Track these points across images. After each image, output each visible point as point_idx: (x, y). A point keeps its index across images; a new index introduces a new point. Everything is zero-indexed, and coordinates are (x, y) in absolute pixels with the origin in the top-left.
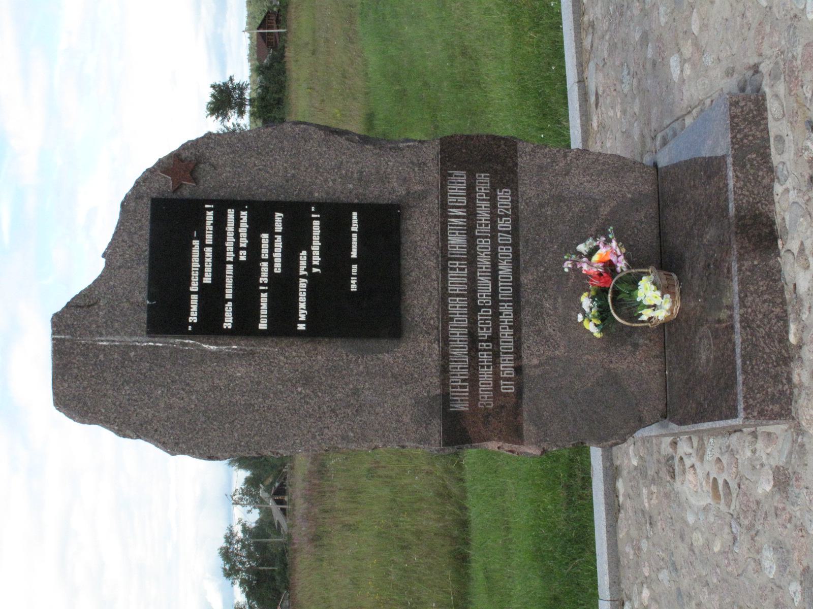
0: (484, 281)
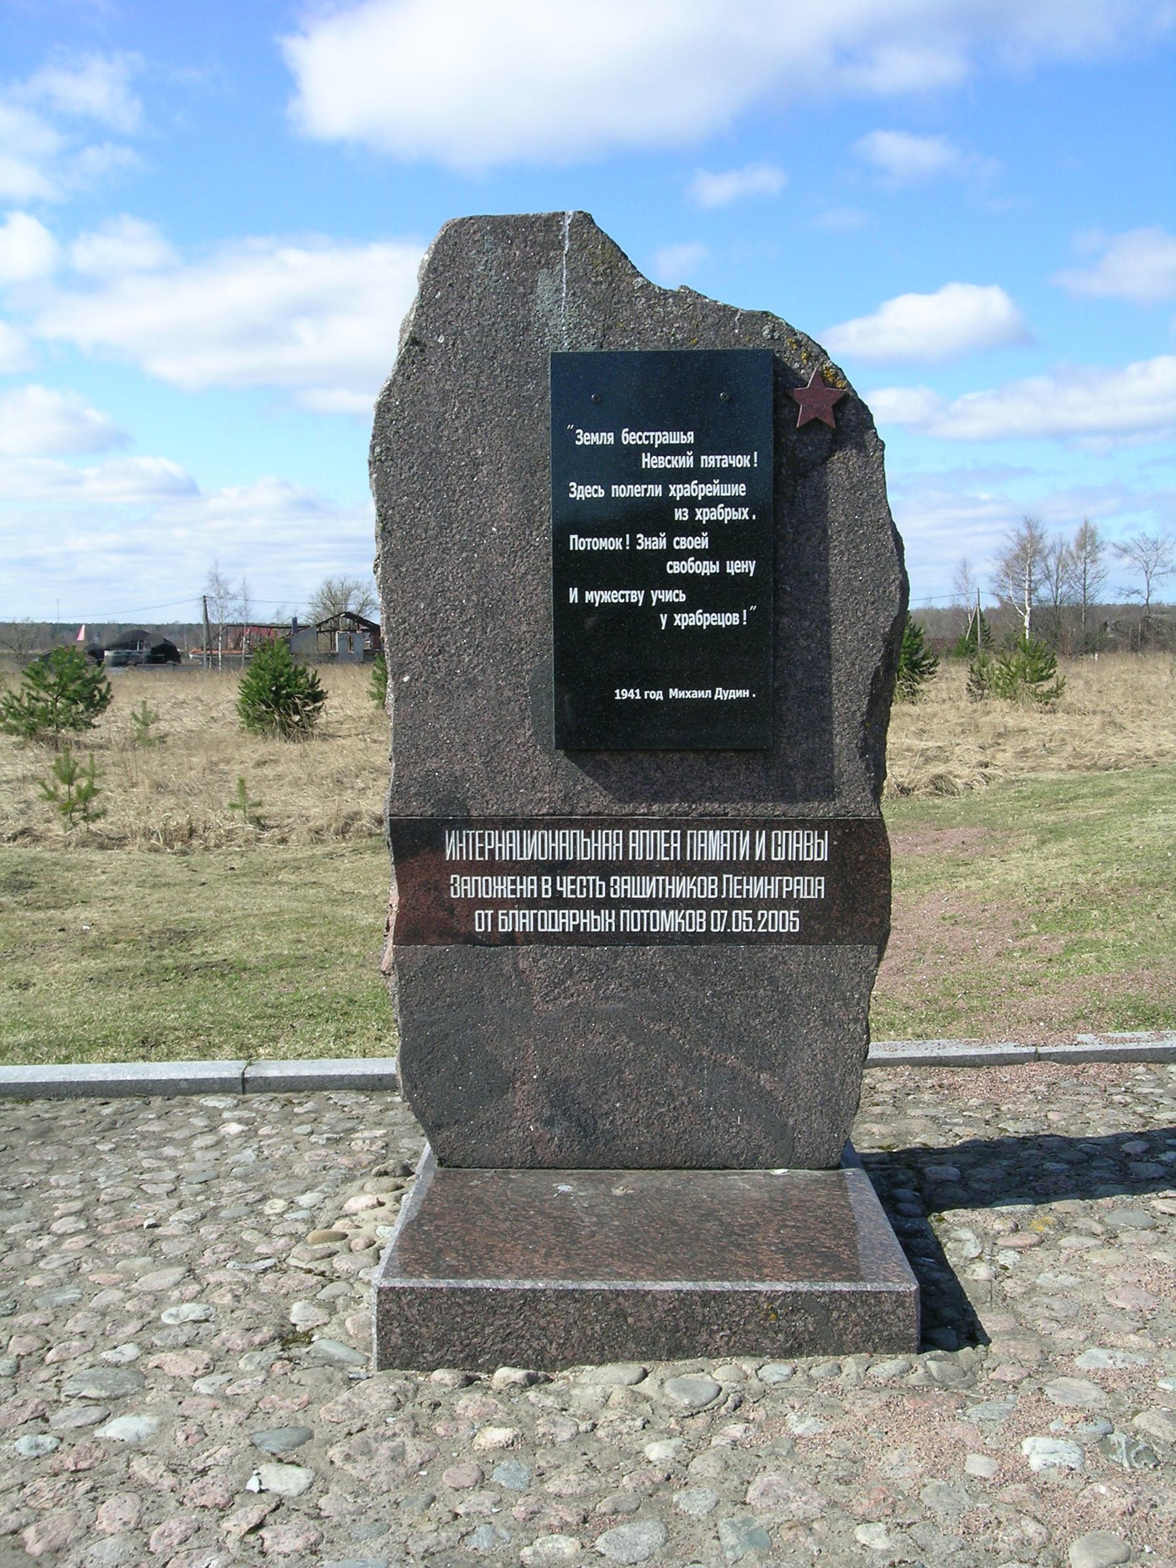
0: (648, 887)
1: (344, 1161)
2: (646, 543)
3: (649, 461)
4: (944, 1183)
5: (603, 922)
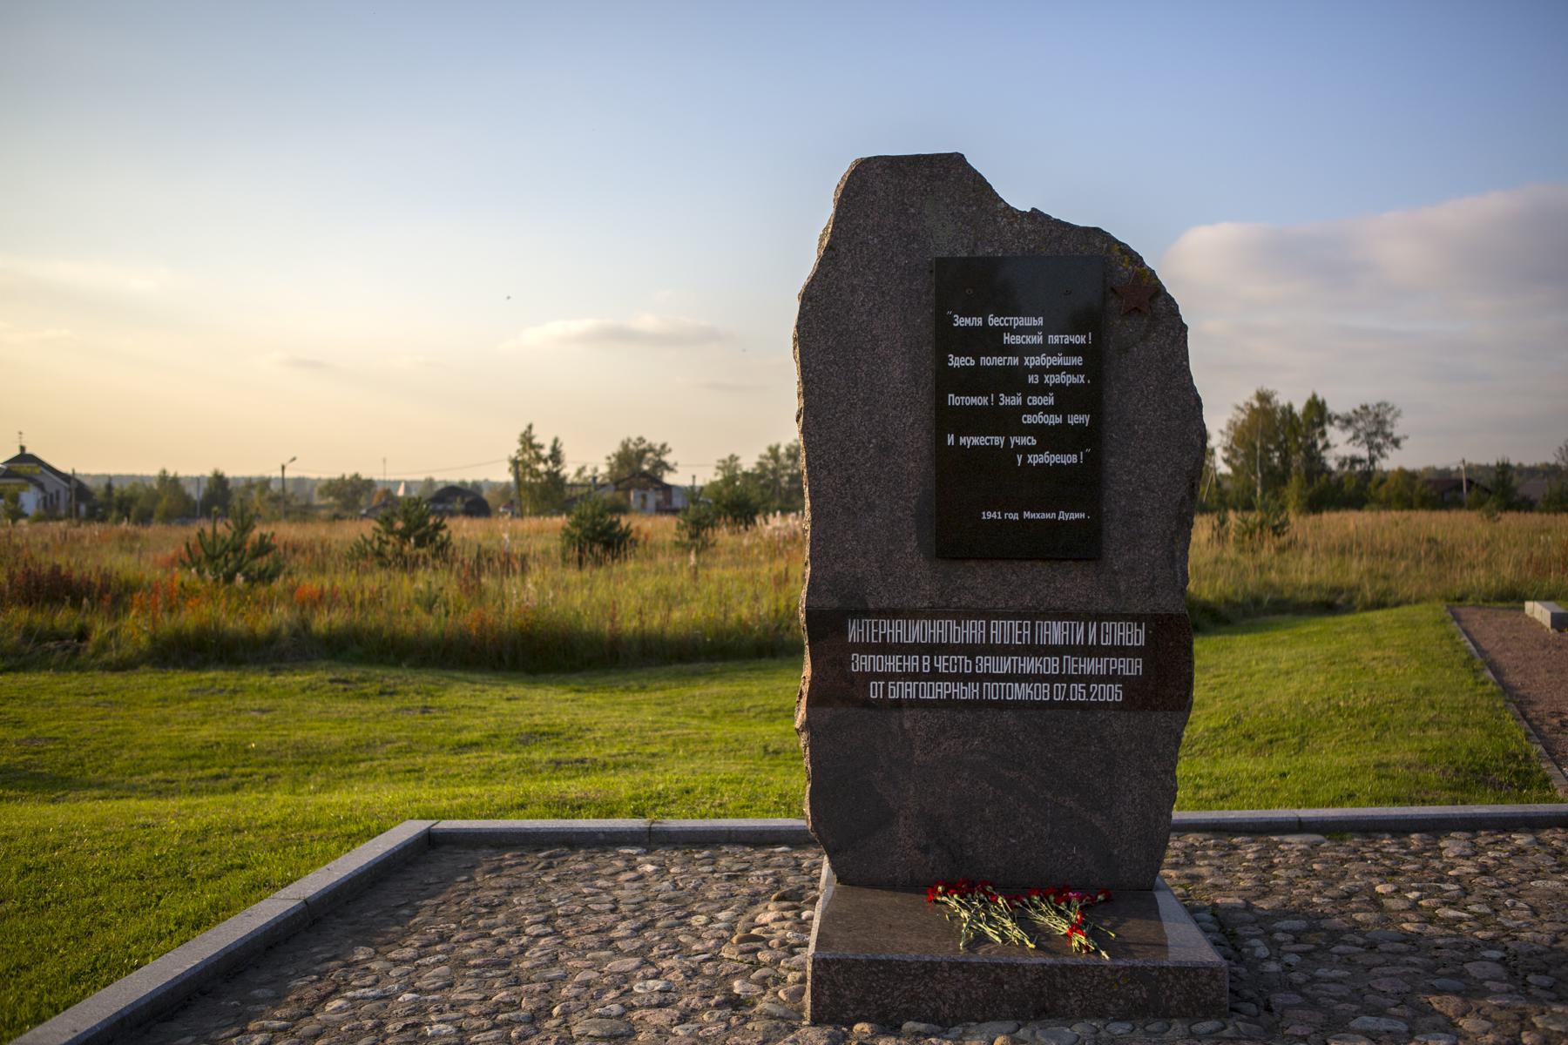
0: (1005, 665)
1: (745, 891)
2: (1005, 401)
3: (1008, 339)
4: (1234, 909)
5: (969, 691)
